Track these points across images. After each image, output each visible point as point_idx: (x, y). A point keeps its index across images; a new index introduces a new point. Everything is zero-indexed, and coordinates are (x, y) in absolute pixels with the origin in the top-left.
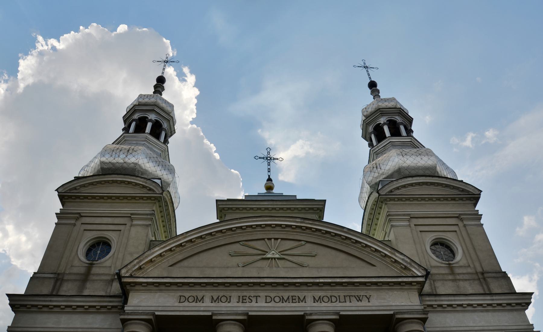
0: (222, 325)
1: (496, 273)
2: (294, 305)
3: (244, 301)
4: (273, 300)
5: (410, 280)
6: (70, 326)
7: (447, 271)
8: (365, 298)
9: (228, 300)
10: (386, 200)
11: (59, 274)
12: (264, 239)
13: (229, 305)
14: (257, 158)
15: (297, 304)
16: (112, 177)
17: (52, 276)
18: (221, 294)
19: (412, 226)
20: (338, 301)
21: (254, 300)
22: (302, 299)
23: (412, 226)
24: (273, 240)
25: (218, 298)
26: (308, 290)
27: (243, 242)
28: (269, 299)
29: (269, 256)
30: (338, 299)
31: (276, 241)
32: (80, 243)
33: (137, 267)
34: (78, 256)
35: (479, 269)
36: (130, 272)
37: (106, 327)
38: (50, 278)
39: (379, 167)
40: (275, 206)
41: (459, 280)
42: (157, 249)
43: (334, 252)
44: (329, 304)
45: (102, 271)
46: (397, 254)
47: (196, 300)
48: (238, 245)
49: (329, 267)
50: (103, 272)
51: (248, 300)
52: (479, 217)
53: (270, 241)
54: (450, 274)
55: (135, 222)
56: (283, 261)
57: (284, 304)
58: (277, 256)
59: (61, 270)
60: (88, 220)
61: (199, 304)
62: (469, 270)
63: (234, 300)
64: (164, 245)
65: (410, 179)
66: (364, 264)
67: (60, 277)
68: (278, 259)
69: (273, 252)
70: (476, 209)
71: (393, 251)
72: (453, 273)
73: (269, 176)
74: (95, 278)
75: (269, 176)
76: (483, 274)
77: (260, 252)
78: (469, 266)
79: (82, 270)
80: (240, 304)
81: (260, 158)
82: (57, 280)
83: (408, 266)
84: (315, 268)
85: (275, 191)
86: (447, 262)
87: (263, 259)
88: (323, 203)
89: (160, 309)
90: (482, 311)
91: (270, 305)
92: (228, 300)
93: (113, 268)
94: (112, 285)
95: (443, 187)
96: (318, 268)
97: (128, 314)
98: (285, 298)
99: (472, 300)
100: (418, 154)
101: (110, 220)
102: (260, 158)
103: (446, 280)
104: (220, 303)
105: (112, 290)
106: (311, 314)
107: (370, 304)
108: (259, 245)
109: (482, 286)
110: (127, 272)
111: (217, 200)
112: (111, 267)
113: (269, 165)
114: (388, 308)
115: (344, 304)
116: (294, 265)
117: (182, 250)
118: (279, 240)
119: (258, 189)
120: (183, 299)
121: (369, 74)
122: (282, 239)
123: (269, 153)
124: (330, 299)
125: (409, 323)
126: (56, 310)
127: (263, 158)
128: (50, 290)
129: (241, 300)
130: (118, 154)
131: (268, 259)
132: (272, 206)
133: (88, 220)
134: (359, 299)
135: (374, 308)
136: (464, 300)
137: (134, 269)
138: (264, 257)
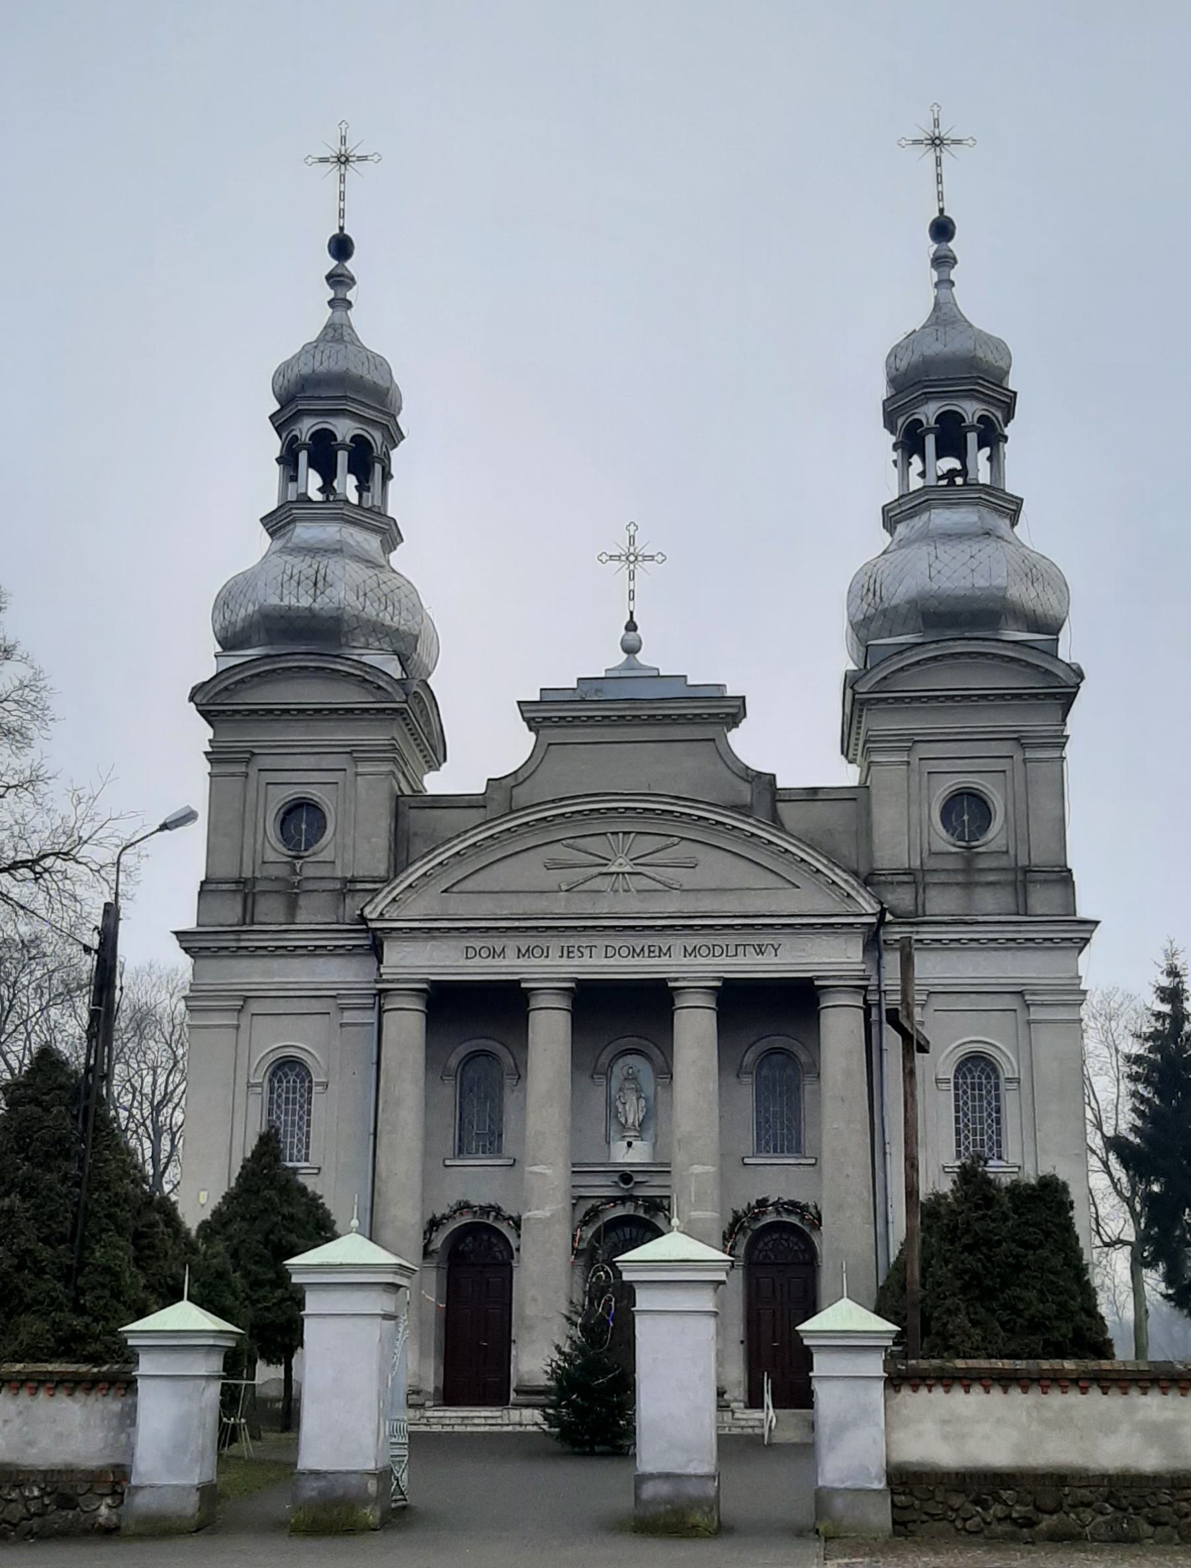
7: (959, 865)
12: (605, 834)
13: (547, 962)
14: (604, 558)
15: (655, 961)
21: (587, 952)
23: (915, 761)
28: (610, 952)
29: (613, 869)
30: (725, 951)
35: (1022, 862)
44: (710, 960)
46: (837, 871)
47: (493, 953)
57: (637, 961)
58: (628, 869)
60: (267, 762)
61: (665, 960)
62: (1004, 862)
63: (554, 952)
68: (629, 873)
69: (621, 860)
78: (1007, 852)
80: (564, 961)
83: (853, 893)
88: (739, 703)
90: (995, 949)
91: (611, 961)
97: (388, 981)
101: (310, 762)
111: (519, 703)
113: (632, 577)
116: (659, 886)
117: (460, 862)
118: (632, 835)
119: (604, 659)
120: (471, 953)
121: (939, 179)
125: (834, 992)
130: (294, 592)
133: (267, 762)
138: (604, 870)
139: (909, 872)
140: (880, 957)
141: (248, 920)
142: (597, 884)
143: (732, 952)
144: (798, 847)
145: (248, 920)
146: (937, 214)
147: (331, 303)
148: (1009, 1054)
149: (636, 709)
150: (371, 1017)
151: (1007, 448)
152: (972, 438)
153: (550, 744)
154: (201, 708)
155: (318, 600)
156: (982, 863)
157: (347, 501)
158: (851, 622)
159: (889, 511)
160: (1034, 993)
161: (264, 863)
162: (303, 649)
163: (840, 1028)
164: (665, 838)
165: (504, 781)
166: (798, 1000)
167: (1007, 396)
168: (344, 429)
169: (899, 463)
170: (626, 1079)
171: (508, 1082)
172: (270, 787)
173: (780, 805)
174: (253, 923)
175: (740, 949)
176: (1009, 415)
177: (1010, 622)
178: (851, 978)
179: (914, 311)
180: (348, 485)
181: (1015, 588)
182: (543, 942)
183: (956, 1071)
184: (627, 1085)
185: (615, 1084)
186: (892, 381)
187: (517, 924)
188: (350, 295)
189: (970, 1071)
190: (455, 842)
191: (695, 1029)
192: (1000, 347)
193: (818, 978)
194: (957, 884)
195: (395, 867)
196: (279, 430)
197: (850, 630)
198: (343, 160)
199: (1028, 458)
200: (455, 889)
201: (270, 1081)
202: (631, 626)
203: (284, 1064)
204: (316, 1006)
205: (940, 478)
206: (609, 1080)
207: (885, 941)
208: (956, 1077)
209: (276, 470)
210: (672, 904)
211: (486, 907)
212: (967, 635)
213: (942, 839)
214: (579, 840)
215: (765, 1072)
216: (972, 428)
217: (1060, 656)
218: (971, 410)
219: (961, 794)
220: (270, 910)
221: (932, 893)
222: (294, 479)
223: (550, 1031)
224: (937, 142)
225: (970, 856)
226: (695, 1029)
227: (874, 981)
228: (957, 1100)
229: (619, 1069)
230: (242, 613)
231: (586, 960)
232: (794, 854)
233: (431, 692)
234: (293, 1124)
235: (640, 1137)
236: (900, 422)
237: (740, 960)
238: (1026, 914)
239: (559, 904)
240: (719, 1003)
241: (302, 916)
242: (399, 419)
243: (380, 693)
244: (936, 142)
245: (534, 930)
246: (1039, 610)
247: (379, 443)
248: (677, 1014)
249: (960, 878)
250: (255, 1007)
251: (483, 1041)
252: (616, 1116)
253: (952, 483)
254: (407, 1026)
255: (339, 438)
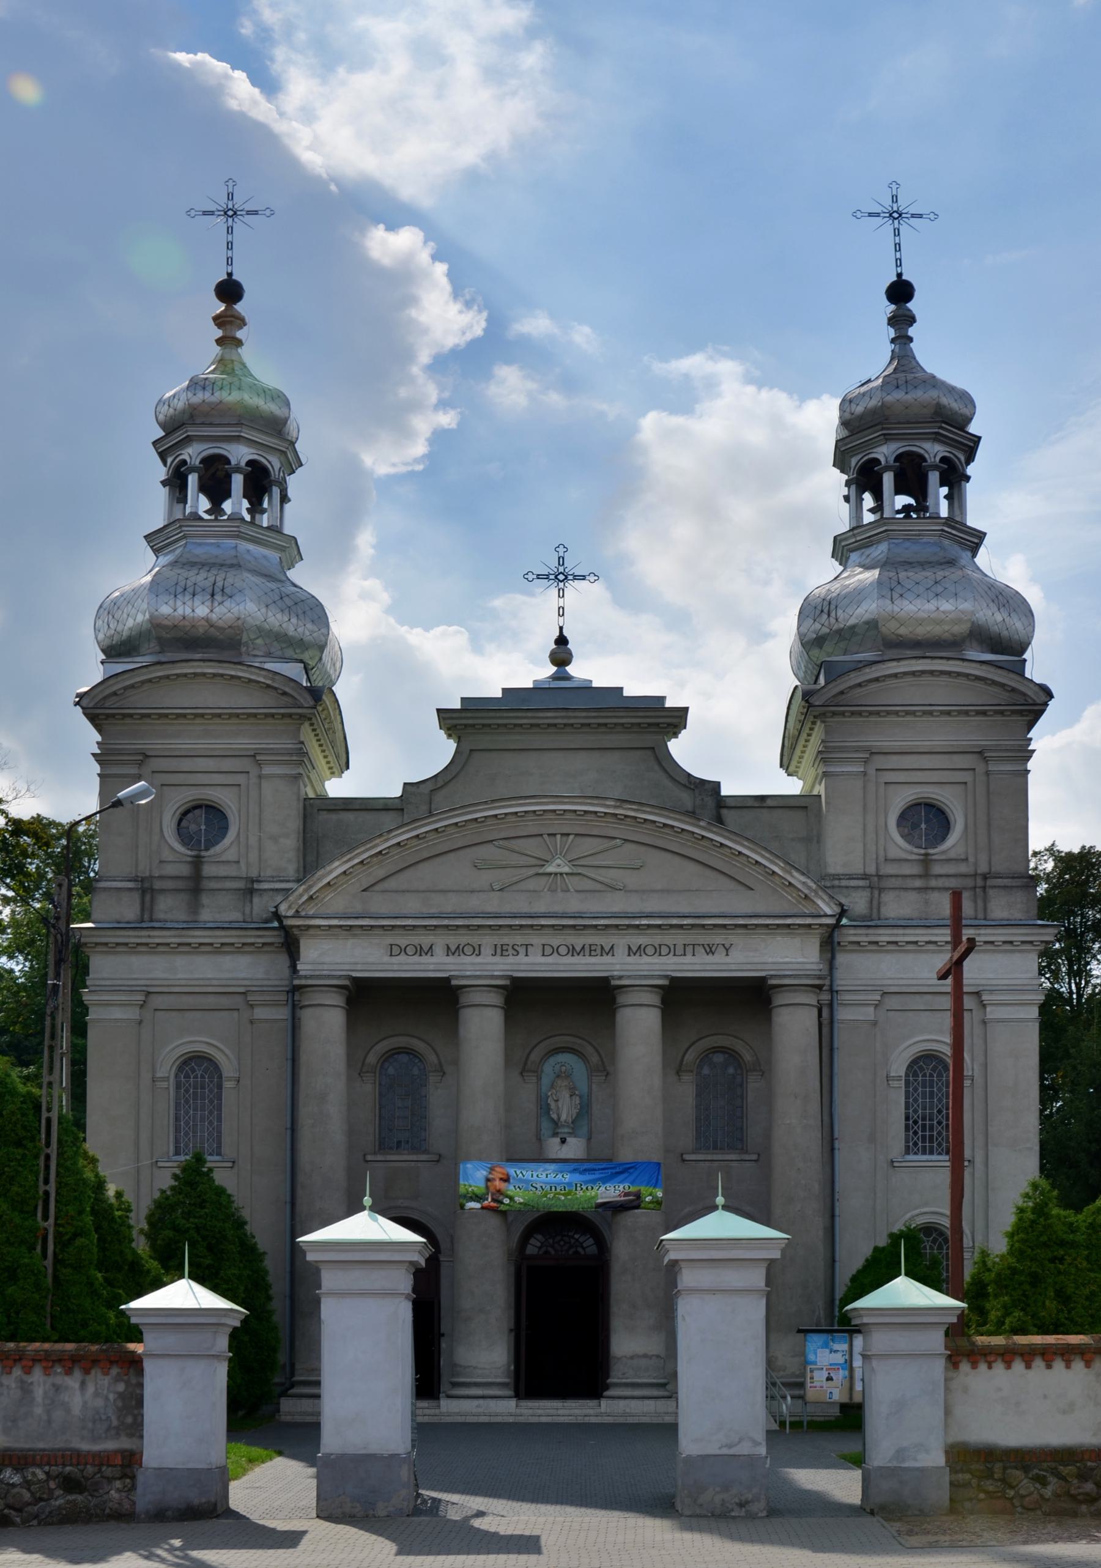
0: (468, 992)
1: (1013, 878)
2: (593, 960)
3: (505, 953)
4: (556, 950)
5: (809, 921)
6: (196, 976)
7: (915, 870)
8: (721, 949)
9: (477, 952)
10: (824, 714)
11: (143, 880)
13: (479, 960)
14: (530, 577)
16: (193, 667)
17: (130, 885)
18: (463, 940)
19: (872, 772)
20: (672, 953)
21: (522, 950)
22: (607, 949)
23: (872, 772)
24: (558, 837)
25: (458, 947)
26: (619, 934)
27: (501, 842)
29: (551, 869)
30: (672, 950)
31: (565, 838)
32: (161, 813)
33: (305, 897)
34: (166, 841)
35: (983, 868)
36: (295, 907)
37: (259, 976)
38: (130, 889)
39: (833, 614)
40: (572, 721)
41: (933, 889)
42: (337, 863)
43: (677, 859)
44: (656, 959)
45: (223, 871)
46: (795, 874)
47: (420, 951)
48: (489, 846)
49: (662, 891)
50: (224, 874)
51: (511, 951)
52: (1028, 754)
53: (552, 838)
54: (920, 876)
55: (267, 770)
56: (577, 878)
57: (576, 959)
58: (566, 869)
59: (144, 870)
61: (425, 959)
62: (963, 868)
64: (349, 856)
65: (895, 664)
66: (732, 885)
67: (146, 885)
69: (558, 861)
70: (1029, 736)
71: (788, 868)
72: (926, 875)
73: (561, 628)
74: (213, 885)
75: (561, 628)
76: (985, 877)
77: (534, 862)
78: (967, 859)
79: (185, 870)
80: (497, 959)
81: (539, 577)
82: (143, 891)
83: (812, 895)
84: (636, 891)
85: (577, 670)
86: (923, 851)
87: (538, 874)
89: (359, 967)
91: (550, 960)
92: (477, 952)
93: (243, 864)
94: (251, 902)
95: (969, 680)
96: (643, 892)
98: (578, 949)
99: (937, 935)
100: (931, 595)
102: (539, 577)
103: (906, 889)
104: (462, 956)
105: (254, 912)
106: (620, 978)
107: (728, 960)
108: (531, 847)
109: (975, 902)
110: (290, 907)
111: (438, 710)
112: (238, 862)
114: (759, 967)
115: (682, 960)
116: (598, 887)
118: (571, 837)
120: (396, 950)
121: (898, 247)
122: (576, 835)
123: (561, 560)
124: (657, 951)
126: (161, 949)
127: (547, 577)
128: (139, 913)
129: (499, 951)
131: (550, 874)
132: (565, 721)
134: (710, 950)
135: (733, 967)
136: (923, 935)
137: (301, 902)
138: (541, 871)
139: (865, 877)
140: (833, 958)
141: (146, 917)
142: (532, 884)
143: (680, 951)
144: (367, 850)
145: (146, 917)
146: (895, 279)
147: (220, 342)
148: (227, 1051)
149: (569, 718)
150: (283, 1013)
151: (969, 487)
152: (934, 477)
153: (471, 750)
154: (89, 711)
155: (217, 610)
156: (937, 869)
157: (243, 519)
158: (801, 641)
159: (841, 541)
160: (991, 992)
161: (161, 862)
162: (198, 656)
163: (794, 1026)
164: (606, 841)
165: (422, 786)
166: (753, 997)
167: (970, 440)
168: (240, 454)
169: (853, 498)
170: (558, 1076)
171: (432, 1079)
172: (165, 788)
173: (724, 812)
174: (151, 921)
175: (689, 949)
176: (970, 459)
177: (975, 644)
178: (807, 976)
179: (874, 359)
180: (236, 504)
181: (981, 613)
182: (475, 940)
183: (907, 1069)
184: (559, 1082)
185: (546, 1081)
186: (845, 423)
187: (446, 922)
188: (239, 334)
189: (921, 1069)
190: (377, 841)
191: (640, 1027)
192: (966, 398)
193: (772, 976)
194: (1017, 887)
195: (304, 867)
196: (163, 455)
197: (798, 647)
198: (231, 213)
199: (991, 499)
200: (376, 888)
201: (176, 1076)
202: (562, 641)
203: (191, 1059)
204: (224, 1001)
205: (898, 512)
206: (539, 1079)
207: (839, 943)
208: (907, 1075)
209: (163, 493)
210: (617, 904)
211: (412, 904)
212: (928, 654)
213: (898, 844)
214: (513, 842)
215: (706, 1071)
216: (935, 467)
217: (1028, 675)
218: (934, 451)
219: (920, 804)
220: (169, 907)
221: (888, 897)
222: (183, 500)
223: (483, 1028)
224: (896, 215)
225: (926, 861)
226: (640, 1027)
227: (827, 982)
228: (907, 1097)
229: (549, 1068)
230: (130, 623)
231: (521, 958)
232: (748, 857)
233: (337, 701)
234: (202, 1120)
235: (573, 1134)
236: (854, 461)
237: (689, 959)
238: (985, 919)
239: (492, 903)
240: (663, 1001)
241: (206, 915)
242: (296, 445)
243: (285, 698)
244: (896, 215)
245: (466, 928)
246: (1005, 633)
247: (277, 468)
248: (775, 1012)
249: (918, 883)
250: (157, 1001)
251: (395, 1039)
252: (548, 1113)
253: (908, 516)
254: (327, 1025)
255: (233, 462)
